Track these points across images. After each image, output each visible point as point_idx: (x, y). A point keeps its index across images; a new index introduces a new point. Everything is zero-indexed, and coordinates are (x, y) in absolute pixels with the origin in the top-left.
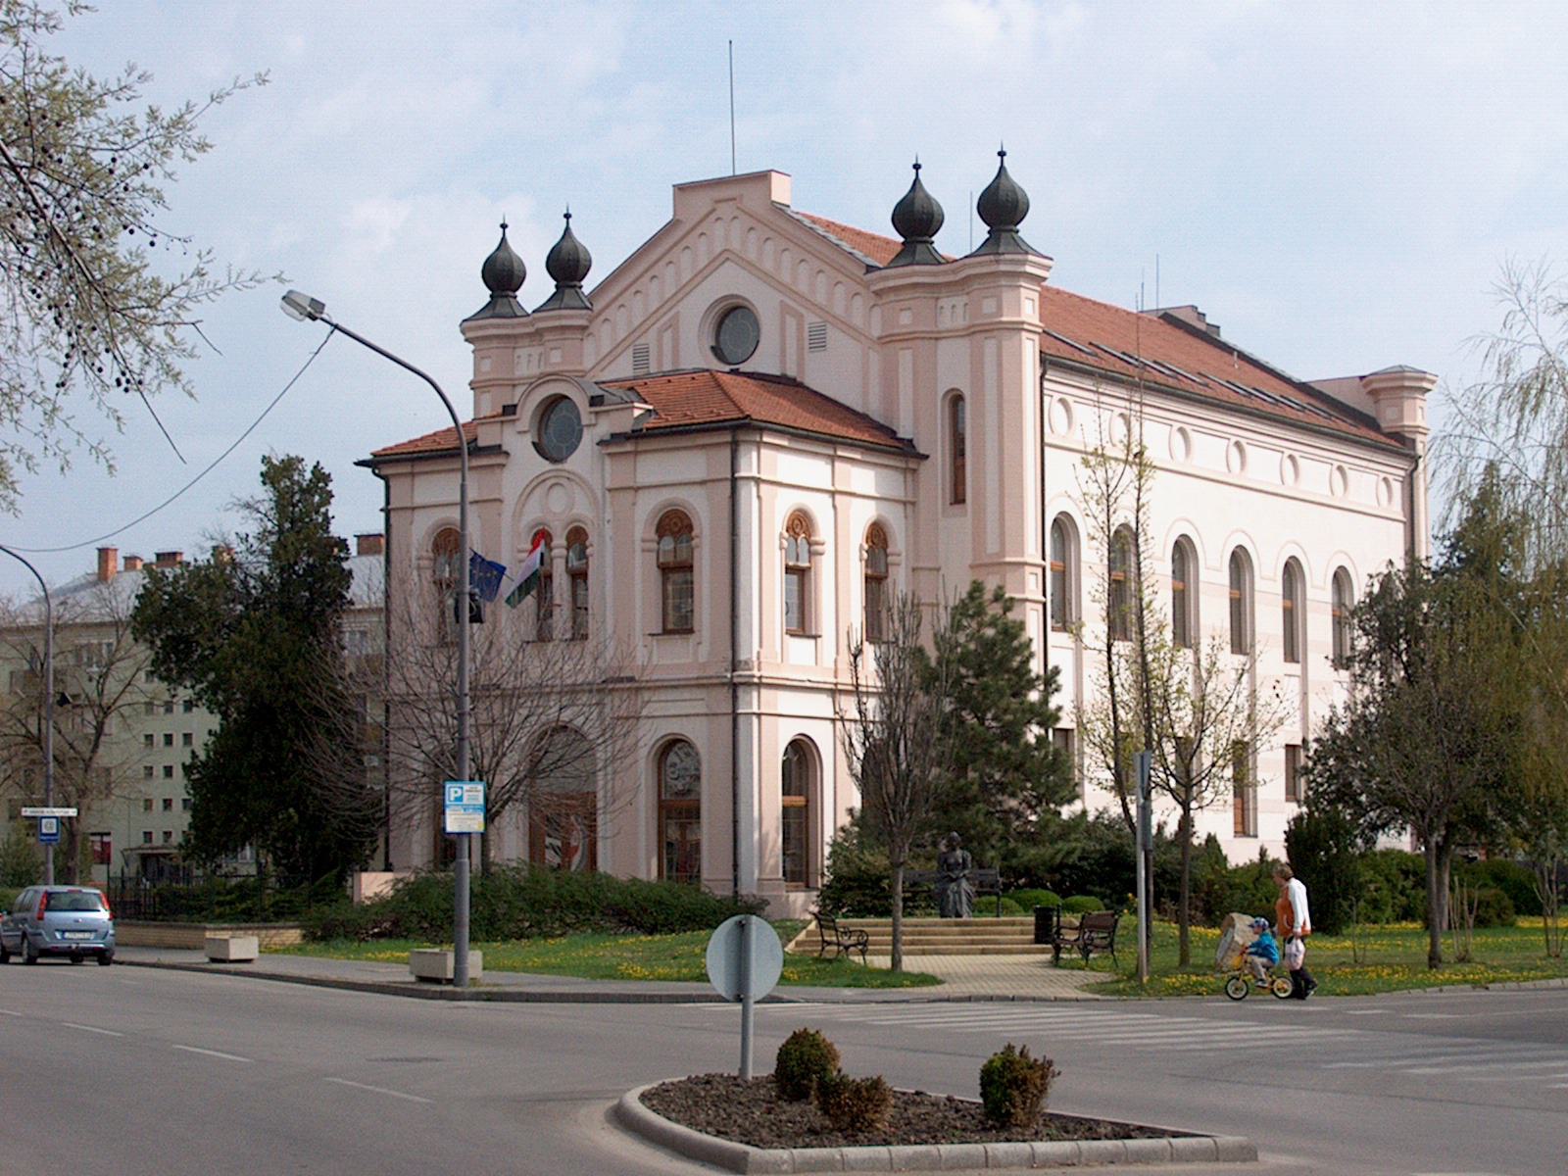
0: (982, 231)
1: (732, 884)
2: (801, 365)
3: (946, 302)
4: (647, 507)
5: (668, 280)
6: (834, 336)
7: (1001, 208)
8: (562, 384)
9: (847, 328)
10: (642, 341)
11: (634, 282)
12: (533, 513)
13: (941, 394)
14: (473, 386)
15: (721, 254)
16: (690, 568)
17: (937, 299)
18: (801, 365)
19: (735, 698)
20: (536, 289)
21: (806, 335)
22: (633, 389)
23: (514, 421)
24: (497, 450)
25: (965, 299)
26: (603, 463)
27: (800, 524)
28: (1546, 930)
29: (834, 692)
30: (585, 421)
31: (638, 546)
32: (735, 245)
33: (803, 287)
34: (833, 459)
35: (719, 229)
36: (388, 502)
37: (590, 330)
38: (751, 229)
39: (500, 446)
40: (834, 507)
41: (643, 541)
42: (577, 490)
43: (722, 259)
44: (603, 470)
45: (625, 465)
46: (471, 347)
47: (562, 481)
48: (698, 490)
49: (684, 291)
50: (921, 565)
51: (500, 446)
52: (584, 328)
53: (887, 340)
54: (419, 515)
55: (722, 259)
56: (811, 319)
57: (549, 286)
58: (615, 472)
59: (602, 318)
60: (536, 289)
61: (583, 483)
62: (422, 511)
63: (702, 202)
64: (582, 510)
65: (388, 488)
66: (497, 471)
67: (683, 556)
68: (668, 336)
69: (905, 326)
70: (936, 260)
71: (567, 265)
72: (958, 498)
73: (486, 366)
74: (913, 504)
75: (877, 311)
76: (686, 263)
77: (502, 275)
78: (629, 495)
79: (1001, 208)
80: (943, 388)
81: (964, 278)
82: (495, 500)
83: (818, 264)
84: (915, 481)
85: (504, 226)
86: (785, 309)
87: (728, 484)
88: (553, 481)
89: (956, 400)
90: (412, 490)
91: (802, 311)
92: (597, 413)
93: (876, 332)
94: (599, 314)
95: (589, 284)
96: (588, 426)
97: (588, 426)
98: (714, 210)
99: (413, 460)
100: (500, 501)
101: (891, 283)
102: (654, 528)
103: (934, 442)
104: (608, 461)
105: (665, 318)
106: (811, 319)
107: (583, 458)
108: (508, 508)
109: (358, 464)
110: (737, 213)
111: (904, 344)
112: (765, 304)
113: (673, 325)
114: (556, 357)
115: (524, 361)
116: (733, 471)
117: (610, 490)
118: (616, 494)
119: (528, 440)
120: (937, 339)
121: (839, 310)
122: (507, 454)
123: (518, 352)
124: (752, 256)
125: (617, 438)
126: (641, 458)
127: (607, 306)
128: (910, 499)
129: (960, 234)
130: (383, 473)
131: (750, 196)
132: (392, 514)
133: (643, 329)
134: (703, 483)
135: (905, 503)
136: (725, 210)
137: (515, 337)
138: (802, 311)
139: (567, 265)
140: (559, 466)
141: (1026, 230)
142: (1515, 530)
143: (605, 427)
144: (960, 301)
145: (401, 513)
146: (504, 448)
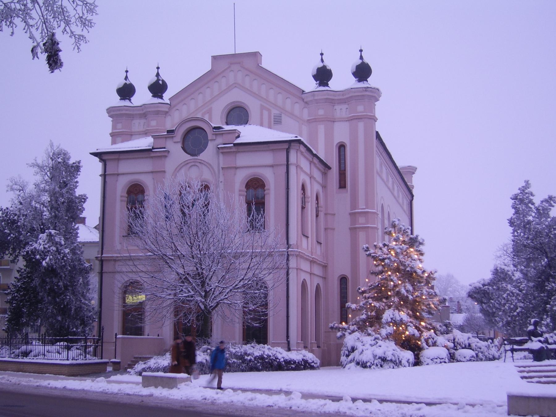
4: (240, 178)
6: (285, 119)
7: (362, 72)
9: (292, 115)
11: (192, 94)
12: (181, 177)
13: (335, 145)
15: (233, 84)
20: (142, 97)
21: (272, 118)
23: (173, 137)
25: (346, 106)
29: (312, 262)
35: (231, 75)
36: (105, 171)
42: (204, 167)
46: (111, 119)
49: (214, 99)
52: (166, 113)
56: (274, 112)
58: (223, 161)
59: (177, 108)
60: (142, 97)
61: (209, 165)
64: (207, 175)
69: (320, 116)
72: (342, 185)
73: (119, 126)
79: (362, 72)
81: (346, 98)
86: (262, 108)
88: (193, 164)
89: (342, 147)
90: (118, 166)
92: (216, 135)
96: (211, 140)
97: (211, 140)
100: (334, 229)
102: (244, 186)
103: (334, 163)
104: (221, 156)
108: (168, 175)
109: (91, 154)
114: (153, 123)
117: (223, 168)
119: (180, 145)
120: (334, 121)
123: (134, 122)
129: (343, 80)
134: (152, 172)
140: (196, 158)
144: (344, 107)
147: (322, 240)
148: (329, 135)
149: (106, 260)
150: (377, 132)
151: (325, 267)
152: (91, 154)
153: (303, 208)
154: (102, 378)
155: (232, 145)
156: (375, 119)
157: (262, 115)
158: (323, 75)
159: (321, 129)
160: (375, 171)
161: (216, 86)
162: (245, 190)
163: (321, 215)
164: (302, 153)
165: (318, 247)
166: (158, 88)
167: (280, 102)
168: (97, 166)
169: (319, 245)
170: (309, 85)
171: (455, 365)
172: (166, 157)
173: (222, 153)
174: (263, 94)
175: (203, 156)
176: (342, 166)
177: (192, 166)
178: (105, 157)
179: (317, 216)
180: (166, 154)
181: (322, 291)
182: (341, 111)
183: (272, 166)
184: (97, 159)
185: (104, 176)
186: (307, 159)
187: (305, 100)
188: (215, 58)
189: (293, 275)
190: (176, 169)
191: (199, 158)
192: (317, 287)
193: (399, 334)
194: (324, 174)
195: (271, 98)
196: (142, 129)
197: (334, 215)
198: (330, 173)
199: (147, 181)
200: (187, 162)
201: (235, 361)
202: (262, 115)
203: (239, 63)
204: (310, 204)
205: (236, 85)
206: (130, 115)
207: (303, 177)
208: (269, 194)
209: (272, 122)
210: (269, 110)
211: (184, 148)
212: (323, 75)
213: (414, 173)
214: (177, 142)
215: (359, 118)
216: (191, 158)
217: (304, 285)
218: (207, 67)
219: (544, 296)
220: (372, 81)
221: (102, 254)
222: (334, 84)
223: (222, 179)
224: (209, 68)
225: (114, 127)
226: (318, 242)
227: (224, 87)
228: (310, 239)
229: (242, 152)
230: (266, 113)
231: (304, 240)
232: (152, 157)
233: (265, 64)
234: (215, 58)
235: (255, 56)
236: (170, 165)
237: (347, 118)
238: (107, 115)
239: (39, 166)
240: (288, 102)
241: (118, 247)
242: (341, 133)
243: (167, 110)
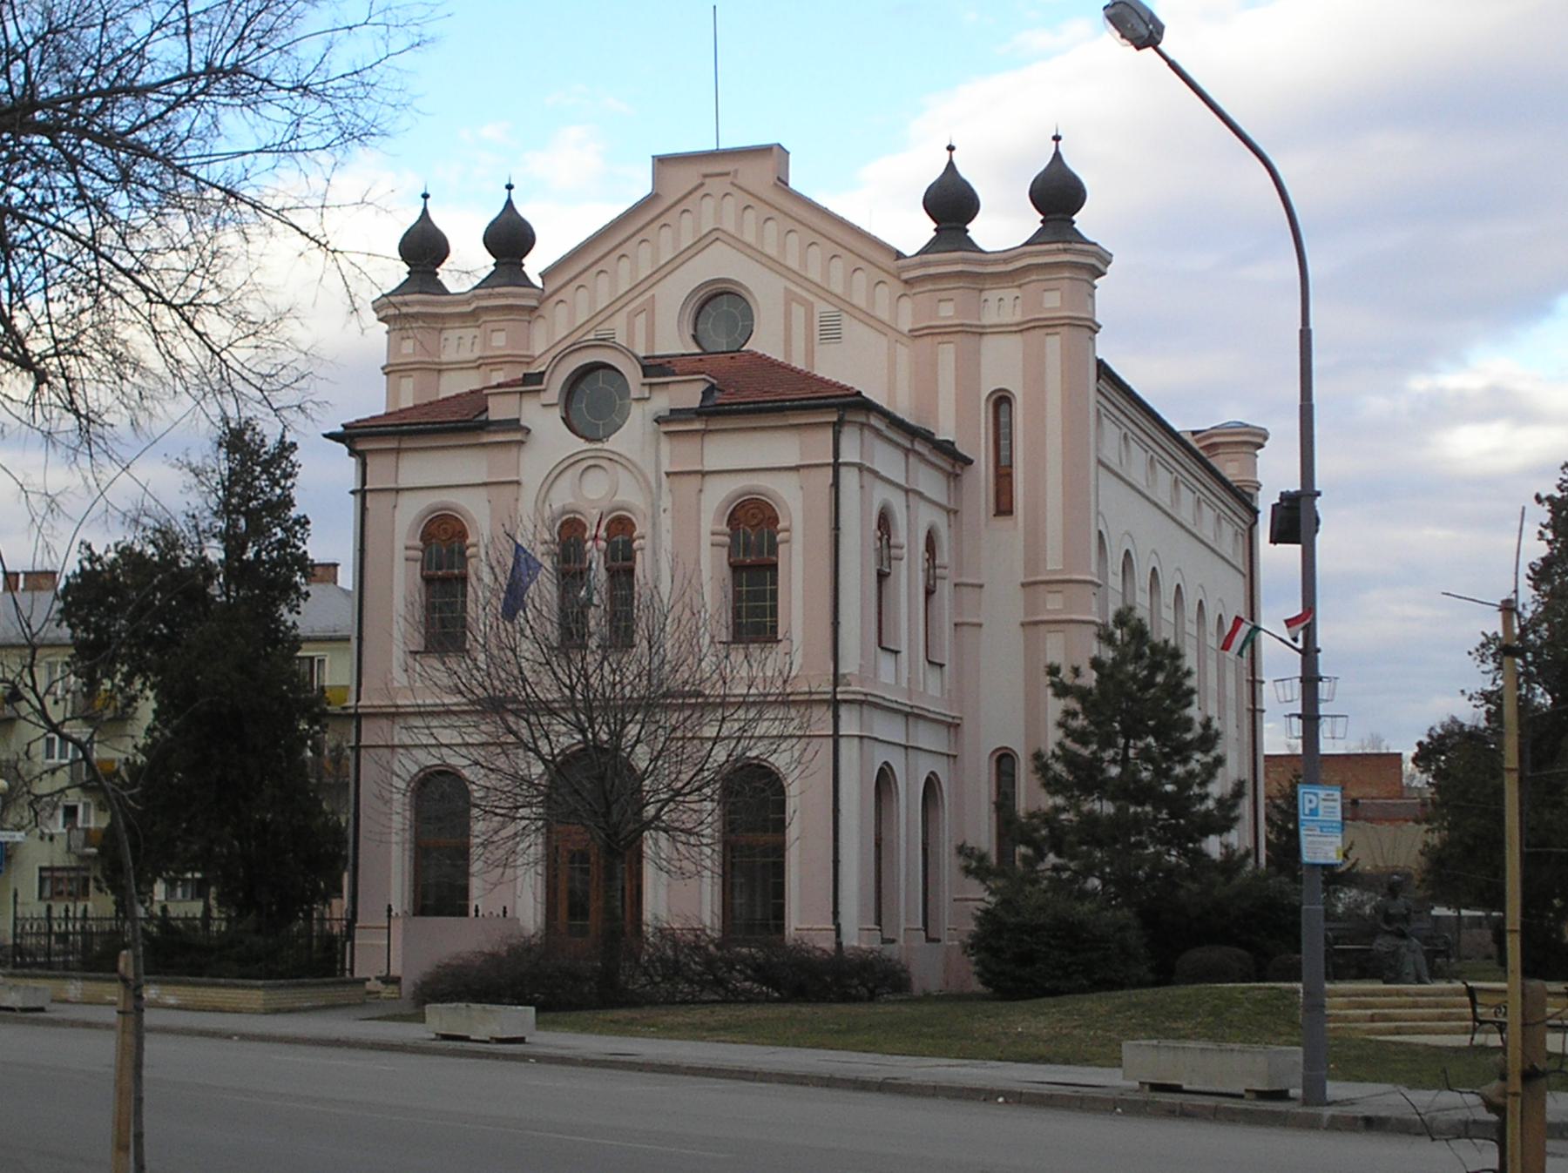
0: (1032, 221)
1: (833, 934)
2: (810, 354)
3: (992, 295)
4: (718, 495)
5: (644, 260)
7: (1057, 195)
8: (608, 351)
9: (868, 318)
10: (606, 325)
12: (562, 497)
14: (388, 371)
17: (981, 290)
18: (810, 354)
19: (836, 718)
20: (468, 263)
23: (539, 391)
24: (514, 425)
25: (1016, 292)
26: (658, 444)
28: (1471, 992)
30: (634, 394)
31: (706, 539)
32: (729, 225)
33: (814, 274)
34: (907, 452)
36: (364, 482)
38: (748, 207)
39: (518, 420)
40: (908, 507)
41: (713, 534)
43: (712, 237)
44: (657, 450)
45: (688, 447)
46: (385, 327)
48: (793, 478)
49: (661, 272)
50: (965, 580)
51: (518, 420)
52: (535, 309)
53: (916, 334)
54: (404, 499)
55: (712, 237)
57: (484, 263)
58: (671, 455)
59: (556, 298)
60: (468, 263)
63: (687, 177)
64: (631, 496)
65: (364, 466)
66: (514, 450)
68: (641, 320)
70: (971, 246)
71: (509, 238)
72: (1004, 507)
73: (408, 347)
74: (956, 512)
75: (906, 304)
76: (666, 244)
77: (423, 248)
78: (695, 481)
79: (1057, 195)
80: (988, 386)
81: (1009, 270)
83: (832, 249)
84: (958, 489)
86: (790, 298)
87: (830, 471)
88: (591, 462)
89: (1002, 401)
91: (811, 298)
92: (651, 385)
93: (905, 328)
94: (551, 296)
95: (534, 265)
98: (702, 185)
99: (403, 433)
101: (932, 270)
103: (980, 451)
104: (663, 439)
105: (641, 299)
106: (821, 307)
107: (634, 434)
109: (325, 436)
110: (730, 189)
111: (946, 338)
112: (765, 292)
113: (649, 309)
115: (453, 341)
116: (836, 454)
117: (668, 474)
118: (676, 479)
119: (557, 413)
120: (981, 334)
121: (860, 299)
122: (528, 431)
123: (446, 334)
124: (749, 237)
125: (676, 415)
126: (709, 439)
128: (952, 506)
129: (1003, 224)
130: (359, 447)
131: (756, 176)
132: (369, 496)
133: (608, 312)
134: (797, 468)
135: (949, 511)
136: (713, 186)
137: (443, 317)
138: (811, 298)
139: (509, 238)
140: (599, 446)
141: (1081, 221)
143: (662, 402)
144: (1009, 294)
145: (382, 496)
146: (523, 423)
147: (945, 655)
148: (968, 370)
151: (953, 727)
152: (325, 436)
153: (882, 576)
156: (1094, 328)
157: (788, 315)
158: (951, 203)
159: (947, 354)
163: (944, 590)
164: (878, 432)
165: (933, 677)
168: (341, 467)
169: (937, 670)
170: (912, 231)
172: (521, 443)
175: (614, 443)
176: (1004, 453)
177: (589, 467)
179: (929, 592)
180: (518, 436)
181: (945, 786)
182: (1002, 306)
184: (342, 448)
185: (362, 493)
186: (897, 445)
189: (849, 750)
191: (606, 446)
192: (928, 781)
194: (954, 477)
196: (466, 354)
197: (981, 586)
198: (968, 476)
202: (788, 315)
204: (904, 563)
206: (435, 316)
207: (881, 494)
209: (817, 337)
210: (810, 307)
211: (566, 421)
212: (951, 203)
213: (1261, 446)
214: (552, 405)
215: (1048, 325)
216: (587, 446)
217: (885, 778)
218: (642, 187)
221: (358, 700)
222: (982, 231)
223: (666, 501)
225: (392, 348)
226: (930, 662)
228: (904, 656)
229: (717, 431)
230: (798, 312)
231: (886, 661)
232: (484, 445)
235: (773, 155)
236: (533, 465)
237: (1018, 324)
239: (192, 470)
241: (400, 679)
242: (1001, 365)
243: (534, 303)
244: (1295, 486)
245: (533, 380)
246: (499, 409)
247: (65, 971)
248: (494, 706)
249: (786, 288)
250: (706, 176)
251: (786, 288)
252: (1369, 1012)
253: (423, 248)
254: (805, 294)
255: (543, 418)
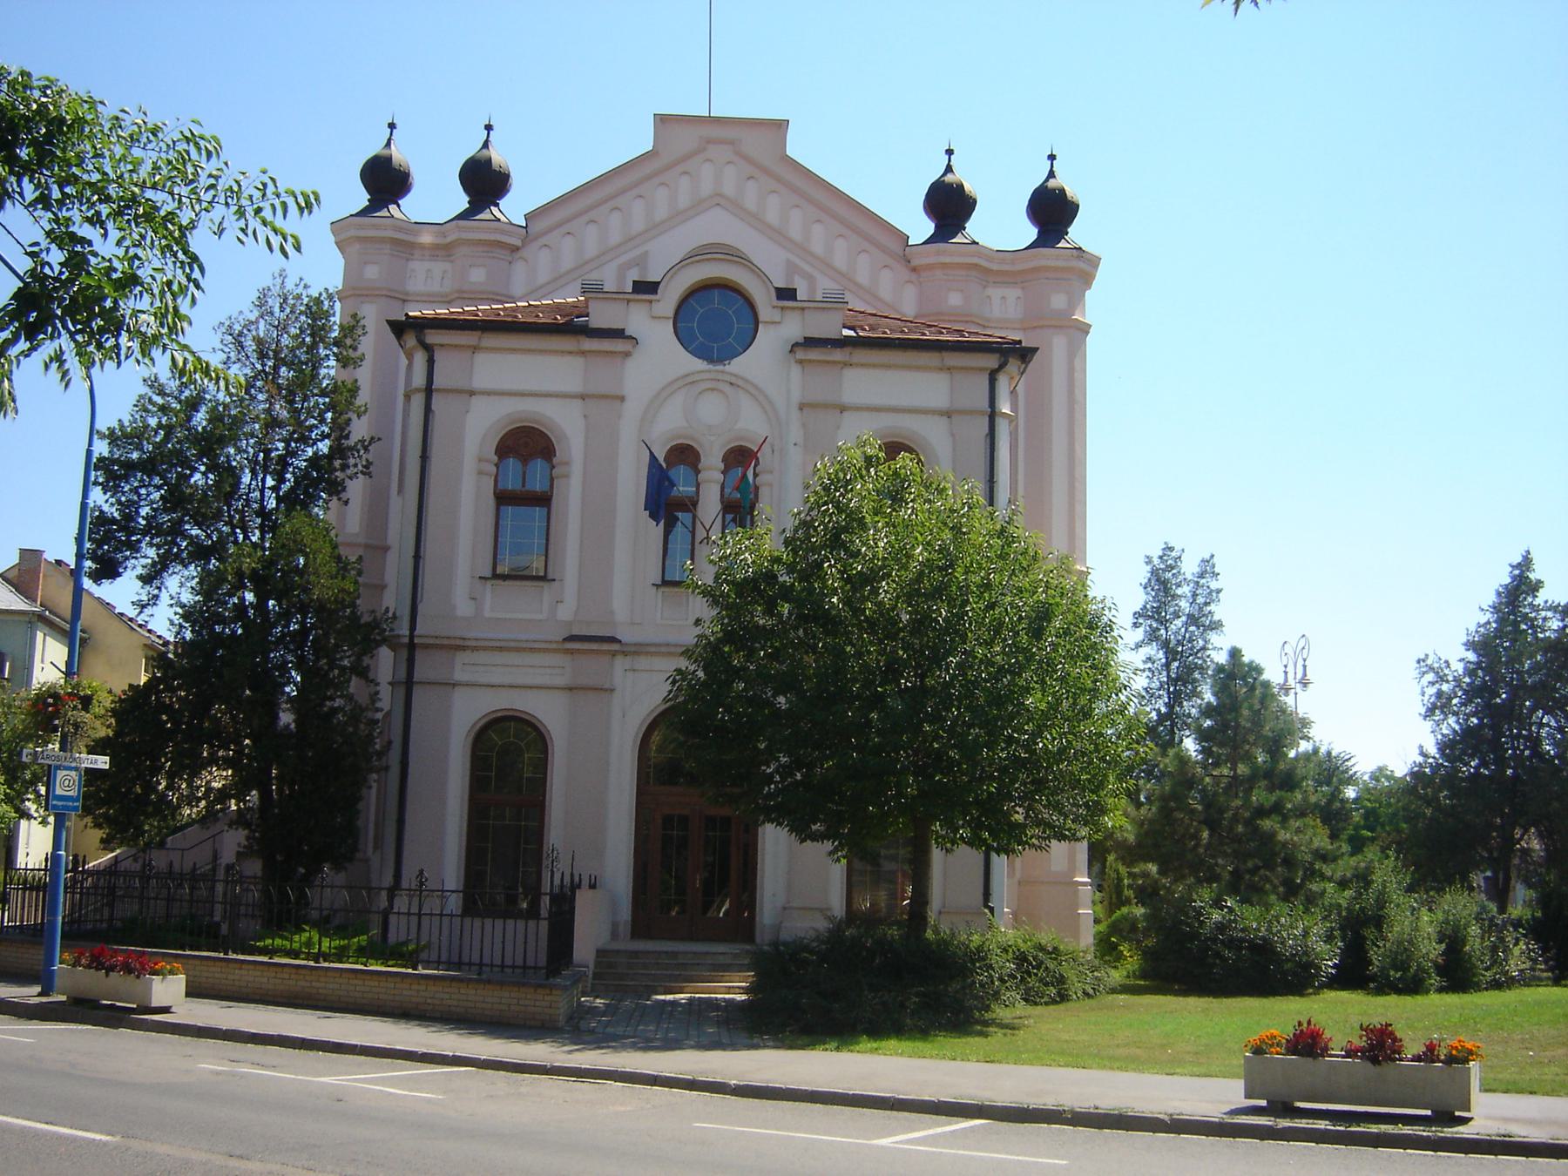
7: (1052, 211)
11: (568, 220)
12: (668, 427)
16: (503, 498)
20: (435, 198)
22: (834, 303)
24: (618, 334)
27: (526, 444)
32: (729, 189)
37: (523, 253)
47: (721, 386)
49: (735, 207)
52: (515, 249)
59: (543, 241)
60: (435, 198)
62: (484, 398)
64: (751, 425)
67: (537, 485)
71: (484, 182)
79: (1052, 211)
82: (826, 406)
85: (1052, 157)
88: (709, 385)
100: (622, 399)
104: (796, 371)
107: (764, 360)
108: (632, 410)
123: (414, 265)
125: (810, 342)
127: (550, 230)
129: (1000, 225)
134: (583, 397)
140: (720, 367)
142: (1535, 587)
149: (427, 646)
150: (565, 640)
154: (1401, 768)
155: (1488, 1113)
158: (949, 205)
160: (44, 999)
161: (662, 195)
162: (722, 466)
166: (484, 182)
167: (840, 260)
170: (920, 227)
171: (491, 501)
172: (627, 354)
173: (801, 362)
174: (795, 232)
175: (738, 365)
178: (433, 337)
183: (583, 397)
187: (915, 262)
188: (663, 121)
190: (659, 394)
193: (183, 768)
195: (818, 247)
199: (568, 425)
200: (690, 379)
201: (337, 319)
203: (731, 143)
205: (718, 200)
208: (567, 476)
212: (949, 205)
218: (642, 141)
219: (332, 699)
220: (1078, 233)
222: (977, 228)
224: (647, 145)
227: (684, 201)
229: (863, 365)
232: (583, 353)
233: (796, 148)
234: (663, 121)
235: (780, 126)
238: (332, 239)
240: (863, 263)
243: (518, 243)
244: (1065, 552)
245: (646, 288)
246: (601, 316)
247: (1121, 992)
248: (578, 641)
249: (788, 261)
250: (709, 141)
251: (788, 261)
252: (276, 960)
253: (385, 180)
254: (807, 268)
255: (653, 328)
